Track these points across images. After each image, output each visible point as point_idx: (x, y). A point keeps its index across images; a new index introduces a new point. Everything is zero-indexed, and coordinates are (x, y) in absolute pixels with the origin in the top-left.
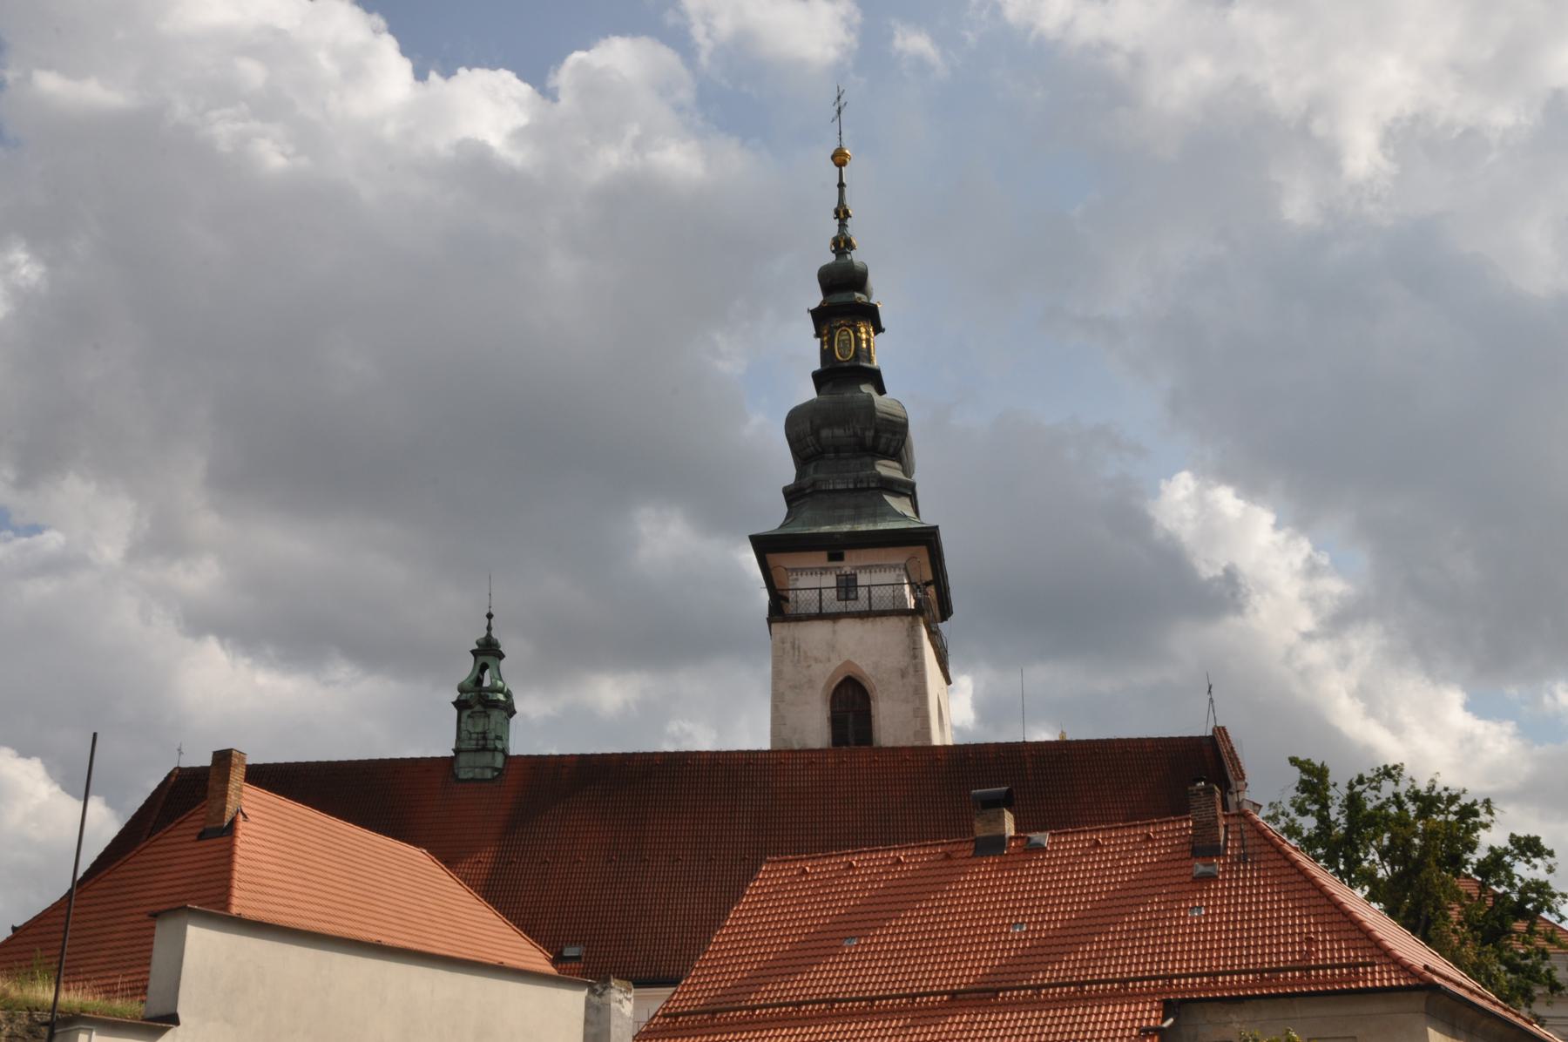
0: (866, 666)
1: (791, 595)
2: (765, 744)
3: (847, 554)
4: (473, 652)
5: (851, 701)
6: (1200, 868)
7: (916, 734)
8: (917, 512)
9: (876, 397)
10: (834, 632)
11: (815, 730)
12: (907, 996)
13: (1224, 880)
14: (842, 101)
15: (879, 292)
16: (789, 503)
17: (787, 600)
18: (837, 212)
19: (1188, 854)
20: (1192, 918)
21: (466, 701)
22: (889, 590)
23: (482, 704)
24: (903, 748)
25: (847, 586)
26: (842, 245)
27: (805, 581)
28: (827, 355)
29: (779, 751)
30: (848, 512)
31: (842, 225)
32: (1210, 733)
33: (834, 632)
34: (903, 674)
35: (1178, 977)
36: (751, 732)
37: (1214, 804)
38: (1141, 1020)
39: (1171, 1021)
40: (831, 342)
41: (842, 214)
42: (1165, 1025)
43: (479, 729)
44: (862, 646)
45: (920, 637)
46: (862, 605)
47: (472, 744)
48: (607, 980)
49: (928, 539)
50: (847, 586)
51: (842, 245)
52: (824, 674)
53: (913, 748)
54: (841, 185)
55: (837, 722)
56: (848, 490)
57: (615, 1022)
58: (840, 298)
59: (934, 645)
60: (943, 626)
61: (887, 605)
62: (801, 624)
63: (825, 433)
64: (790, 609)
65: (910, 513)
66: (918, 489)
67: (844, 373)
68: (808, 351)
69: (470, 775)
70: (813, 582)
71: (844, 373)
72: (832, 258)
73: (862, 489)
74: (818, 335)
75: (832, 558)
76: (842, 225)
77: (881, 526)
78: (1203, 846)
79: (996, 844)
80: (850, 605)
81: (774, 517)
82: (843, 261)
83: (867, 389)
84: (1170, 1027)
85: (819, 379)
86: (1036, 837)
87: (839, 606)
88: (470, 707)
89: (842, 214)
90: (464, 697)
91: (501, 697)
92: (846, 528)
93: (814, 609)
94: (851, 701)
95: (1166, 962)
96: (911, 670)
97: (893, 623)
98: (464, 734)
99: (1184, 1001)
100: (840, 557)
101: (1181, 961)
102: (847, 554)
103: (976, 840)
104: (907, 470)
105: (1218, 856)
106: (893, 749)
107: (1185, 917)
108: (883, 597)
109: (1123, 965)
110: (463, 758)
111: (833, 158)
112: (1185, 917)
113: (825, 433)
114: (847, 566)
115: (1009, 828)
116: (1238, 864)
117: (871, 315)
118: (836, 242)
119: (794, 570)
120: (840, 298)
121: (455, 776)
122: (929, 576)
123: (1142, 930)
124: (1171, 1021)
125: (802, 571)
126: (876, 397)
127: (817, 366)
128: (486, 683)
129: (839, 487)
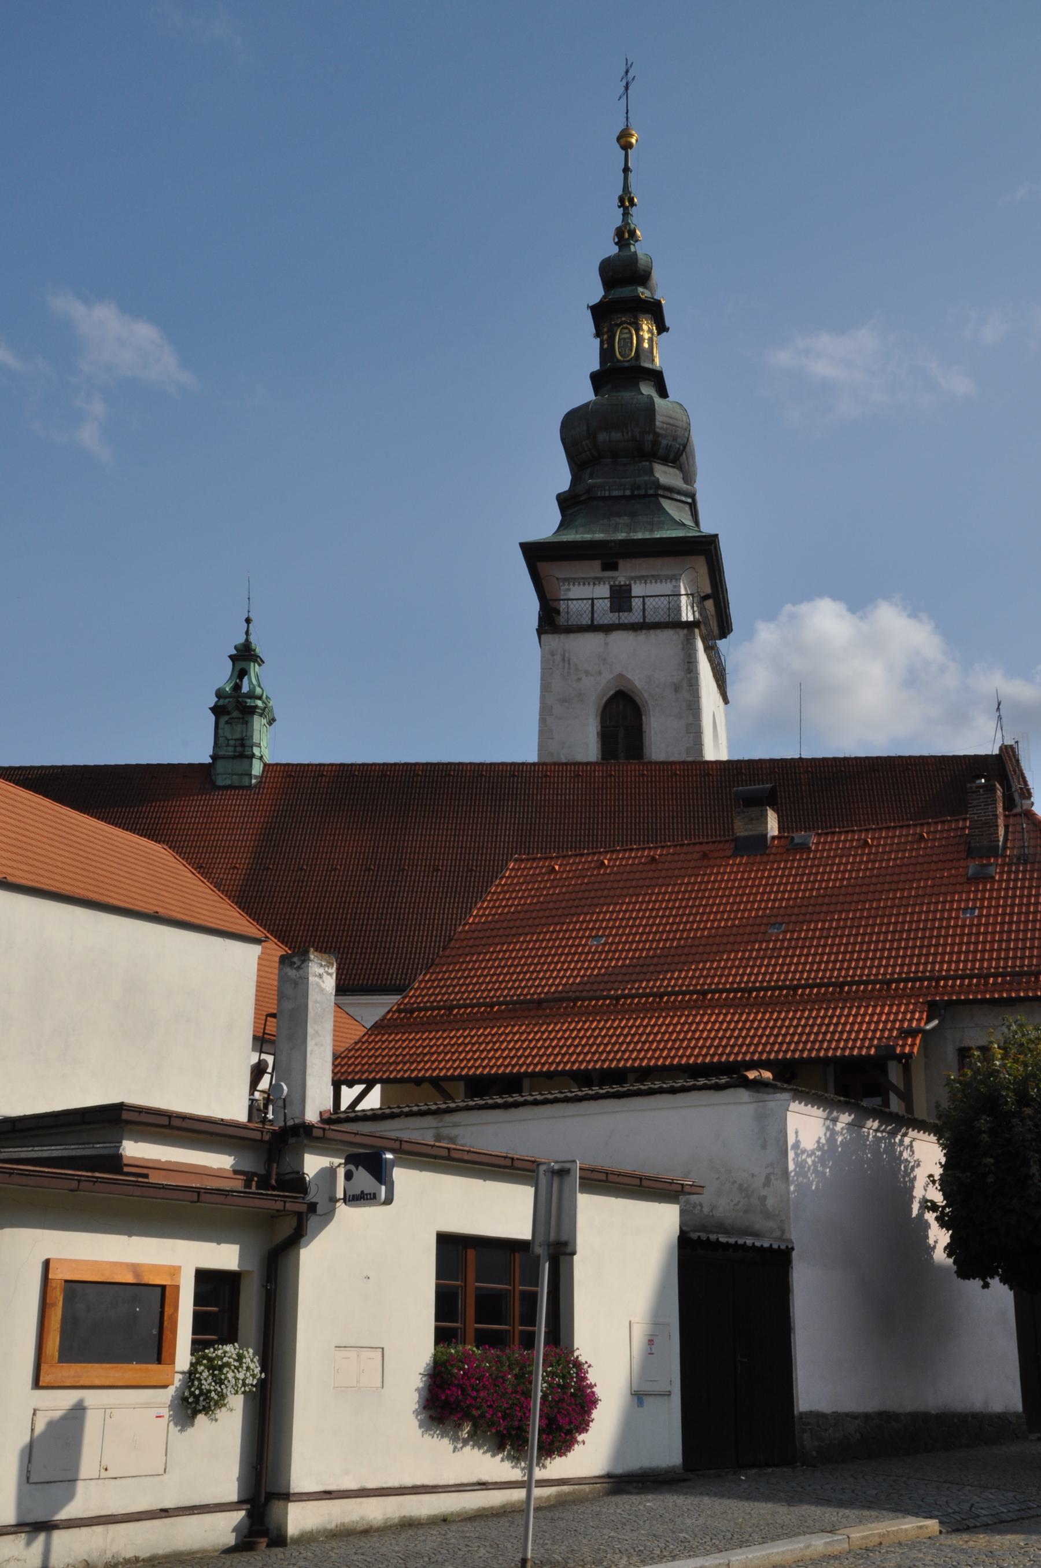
0: (638, 680)
1: (562, 606)
2: (529, 754)
3: (621, 563)
4: (231, 657)
5: (623, 716)
6: (972, 867)
7: (688, 750)
8: (697, 523)
9: (658, 401)
10: (606, 644)
11: (585, 744)
12: (654, 995)
13: (1001, 881)
14: (630, 75)
15: (663, 287)
16: (563, 510)
17: (558, 612)
18: (621, 200)
19: (964, 855)
20: (965, 920)
21: (224, 707)
22: (664, 601)
23: (235, 710)
24: (673, 763)
25: (621, 598)
26: (625, 236)
27: (577, 591)
28: (606, 354)
29: (543, 764)
30: (626, 520)
31: (626, 214)
32: (996, 752)
33: (606, 644)
34: (677, 689)
35: (946, 978)
36: (517, 743)
37: (994, 802)
38: (902, 1021)
39: (935, 1022)
40: (611, 340)
41: (626, 202)
42: (928, 1027)
43: (238, 736)
44: (634, 658)
45: (694, 650)
46: (635, 616)
47: (230, 751)
48: (306, 953)
49: (706, 549)
50: (621, 598)
51: (625, 236)
52: (595, 688)
53: (684, 763)
54: (626, 170)
55: (607, 737)
56: (624, 497)
57: (313, 996)
58: (624, 292)
59: (710, 660)
60: (721, 644)
61: (661, 617)
62: (572, 636)
63: (602, 437)
64: (562, 620)
65: (689, 522)
66: (698, 497)
67: (622, 375)
68: (588, 356)
69: (228, 782)
70: (586, 594)
71: (622, 375)
72: (615, 250)
73: (640, 496)
74: (598, 334)
75: (606, 567)
76: (626, 214)
77: (658, 535)
78: (980, 847)
79: (759, 843)
80: (622, 614)
81: (545, 523)
82: (626, 253)
83: (647, 389)
84: (934, 1029)
85: (598, 380)
86: (799, 836)
87: (611, 618)
88: (228, 713)
89: (626, 202)
90: (222, 702)
91: (259, 703)
92: (621, 536)
93: (586, 620)
94: (623, 716)
95: (933, 963)
96: (685, 685)
97: (667, 635)
98: (221, 740)
99: (950, 1003)
100: (614, 567)
101: (950, 962)
102: (621, 563)
103: (736, 840)
104: (688, 477)
105: (996, 857)
106: (663, 763)
107: (957, 918)
108: (656, 610)
109: (886, 966)
110: (220, 765)
111: (619, 139)
112: (957, 918)
113: (602, 437)
114: (621, 577)
115: (773, 826)
116: (1018, 864)
117: (655, 311)
118: (619, 232)
119: (566, 580)
120: (624, 292)
121: (212, 783)
122: (708, 590)
123: (899, 907)
124: (935, 1022)
125: (574, 581)
126: (658, 401)
127: (596, 366)
128: (245, 689)
129: (615, 493)
